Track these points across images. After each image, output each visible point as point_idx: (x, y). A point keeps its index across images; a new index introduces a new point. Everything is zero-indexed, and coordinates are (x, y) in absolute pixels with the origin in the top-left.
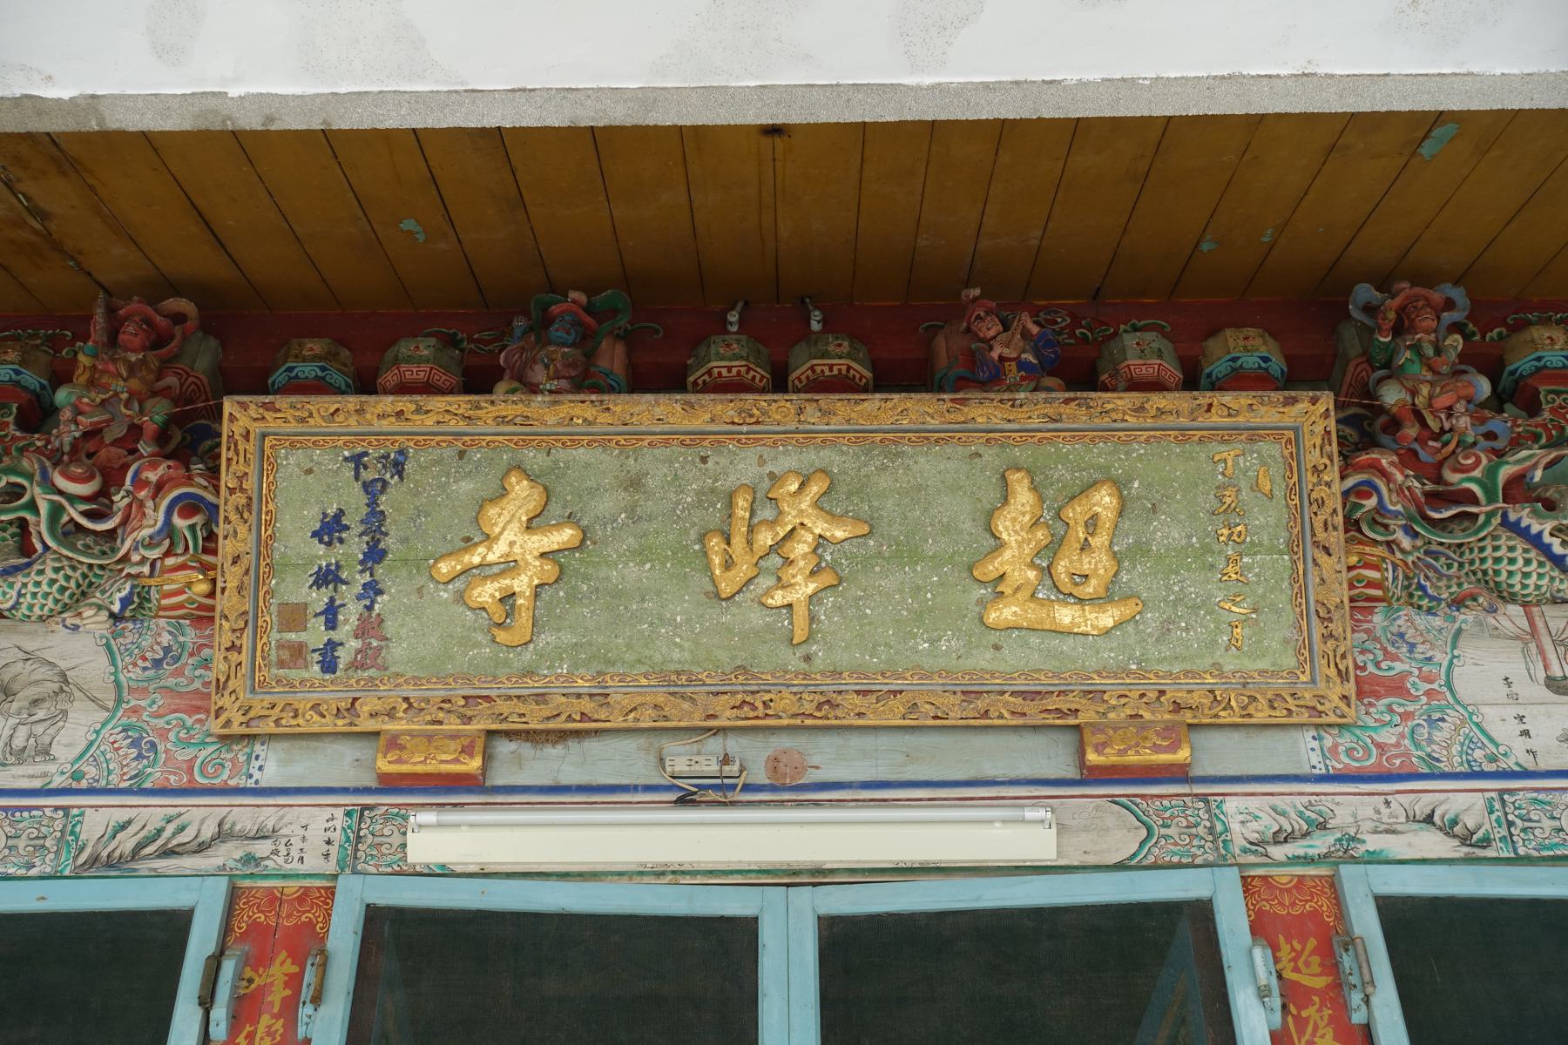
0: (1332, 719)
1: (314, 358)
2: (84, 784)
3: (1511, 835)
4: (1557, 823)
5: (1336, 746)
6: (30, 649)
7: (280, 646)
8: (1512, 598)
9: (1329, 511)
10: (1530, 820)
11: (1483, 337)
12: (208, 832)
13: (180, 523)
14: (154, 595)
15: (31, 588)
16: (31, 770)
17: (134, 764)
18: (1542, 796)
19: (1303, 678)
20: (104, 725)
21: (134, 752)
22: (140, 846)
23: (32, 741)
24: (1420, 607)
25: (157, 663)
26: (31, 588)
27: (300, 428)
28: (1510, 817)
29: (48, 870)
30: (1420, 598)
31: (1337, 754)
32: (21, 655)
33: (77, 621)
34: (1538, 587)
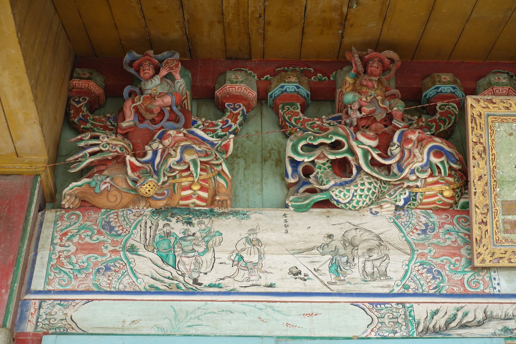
1: (449, 83)
2: (411, 291)
6: (356, 224)
7: (505, 222)
12: (480, 316)
13: (434, 160)
14: (419, 196)
15: (359, 192)
16: (381, 284)
17: (433, 281)
20: (410, 261)
21: (430, 276)
22: (447, 324)
23: (375, 269)
25: (424, 232)
26: (359, 192)
27: (507, 112)
29: (405, 334)
32: (352, 227)
33: (378, 210)
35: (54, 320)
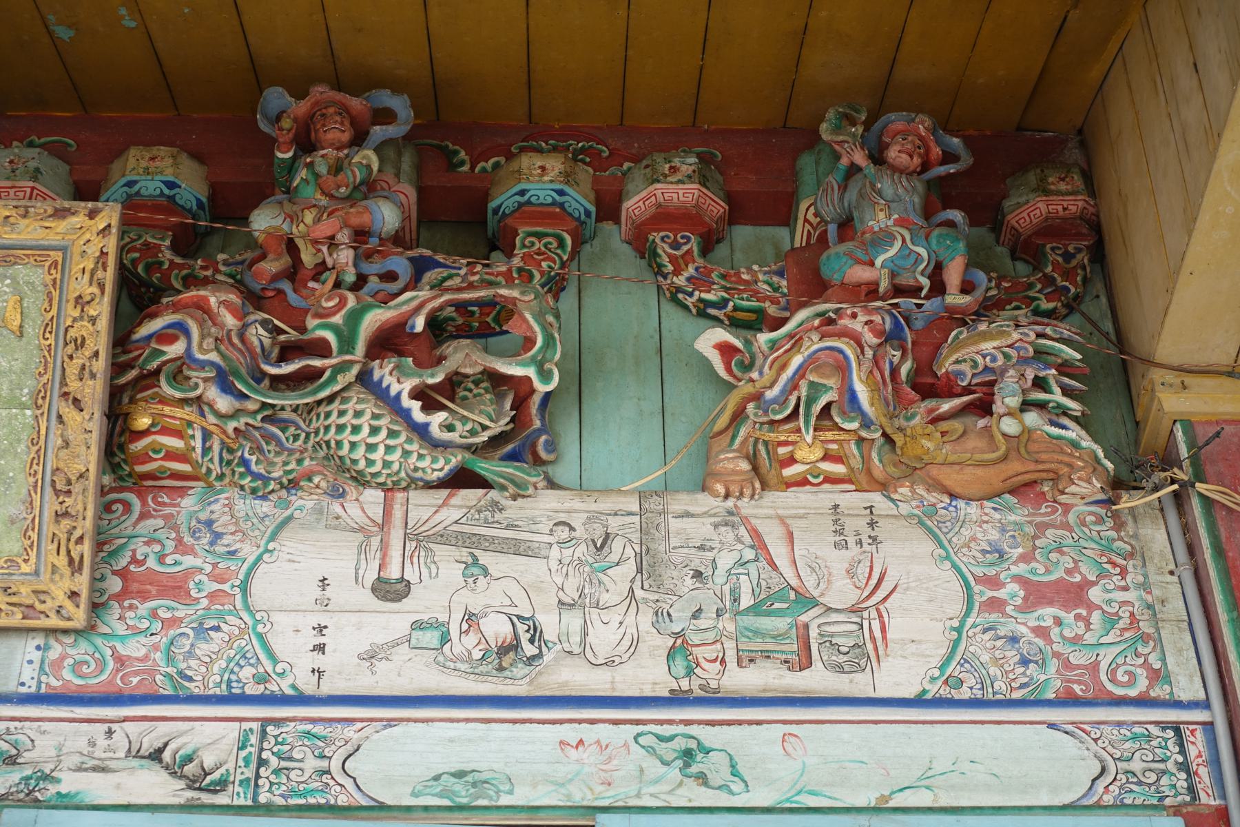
0: (54, 622)
2: (965, 693)
3: (258, 776)
4: (324, 764)
5: (63, 658)
8: (361, 480)
9: (88, 353)
10: (291, 759)
11: (472, 168)
18: (318, 729)
19: (25, 568)
24: (242, 488)
28: (265, 755)
30: (242, 475)
31: (61, 667)
34: (387, 464)
35: (300, 773)
